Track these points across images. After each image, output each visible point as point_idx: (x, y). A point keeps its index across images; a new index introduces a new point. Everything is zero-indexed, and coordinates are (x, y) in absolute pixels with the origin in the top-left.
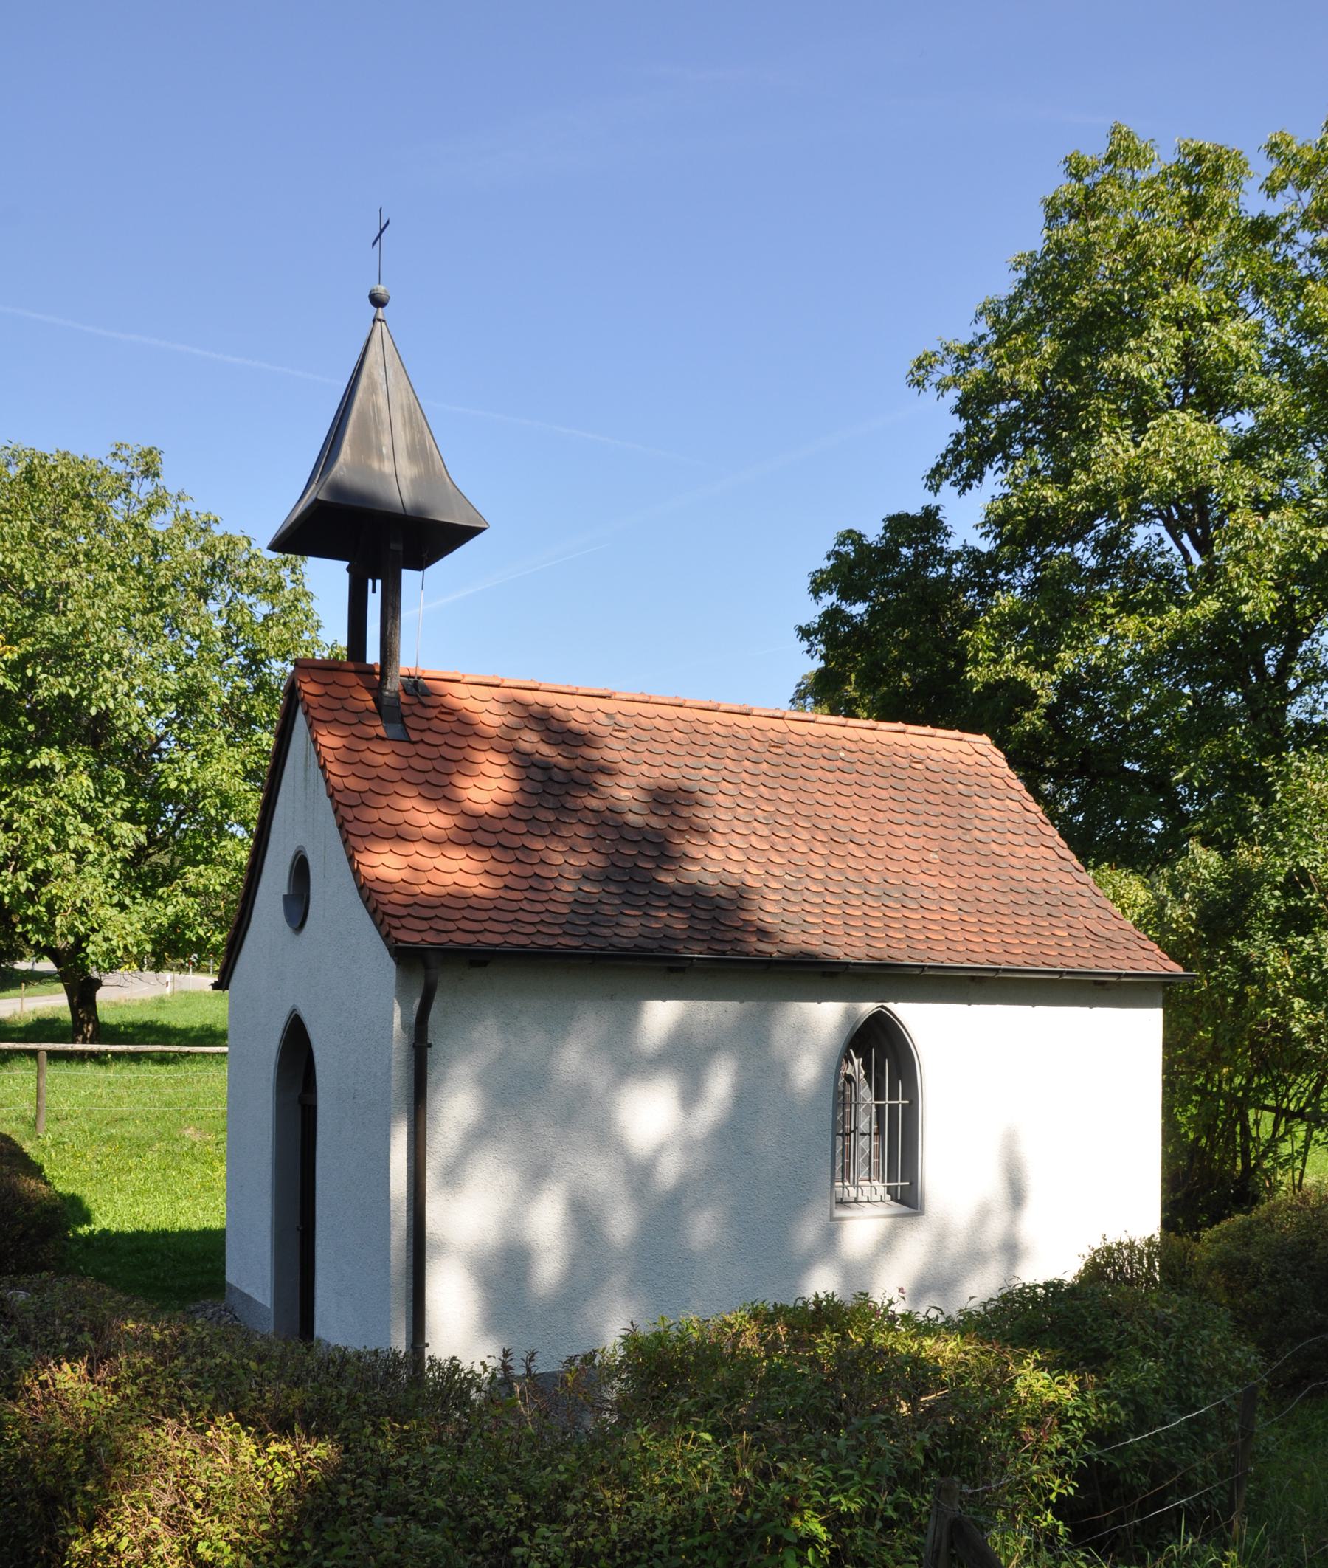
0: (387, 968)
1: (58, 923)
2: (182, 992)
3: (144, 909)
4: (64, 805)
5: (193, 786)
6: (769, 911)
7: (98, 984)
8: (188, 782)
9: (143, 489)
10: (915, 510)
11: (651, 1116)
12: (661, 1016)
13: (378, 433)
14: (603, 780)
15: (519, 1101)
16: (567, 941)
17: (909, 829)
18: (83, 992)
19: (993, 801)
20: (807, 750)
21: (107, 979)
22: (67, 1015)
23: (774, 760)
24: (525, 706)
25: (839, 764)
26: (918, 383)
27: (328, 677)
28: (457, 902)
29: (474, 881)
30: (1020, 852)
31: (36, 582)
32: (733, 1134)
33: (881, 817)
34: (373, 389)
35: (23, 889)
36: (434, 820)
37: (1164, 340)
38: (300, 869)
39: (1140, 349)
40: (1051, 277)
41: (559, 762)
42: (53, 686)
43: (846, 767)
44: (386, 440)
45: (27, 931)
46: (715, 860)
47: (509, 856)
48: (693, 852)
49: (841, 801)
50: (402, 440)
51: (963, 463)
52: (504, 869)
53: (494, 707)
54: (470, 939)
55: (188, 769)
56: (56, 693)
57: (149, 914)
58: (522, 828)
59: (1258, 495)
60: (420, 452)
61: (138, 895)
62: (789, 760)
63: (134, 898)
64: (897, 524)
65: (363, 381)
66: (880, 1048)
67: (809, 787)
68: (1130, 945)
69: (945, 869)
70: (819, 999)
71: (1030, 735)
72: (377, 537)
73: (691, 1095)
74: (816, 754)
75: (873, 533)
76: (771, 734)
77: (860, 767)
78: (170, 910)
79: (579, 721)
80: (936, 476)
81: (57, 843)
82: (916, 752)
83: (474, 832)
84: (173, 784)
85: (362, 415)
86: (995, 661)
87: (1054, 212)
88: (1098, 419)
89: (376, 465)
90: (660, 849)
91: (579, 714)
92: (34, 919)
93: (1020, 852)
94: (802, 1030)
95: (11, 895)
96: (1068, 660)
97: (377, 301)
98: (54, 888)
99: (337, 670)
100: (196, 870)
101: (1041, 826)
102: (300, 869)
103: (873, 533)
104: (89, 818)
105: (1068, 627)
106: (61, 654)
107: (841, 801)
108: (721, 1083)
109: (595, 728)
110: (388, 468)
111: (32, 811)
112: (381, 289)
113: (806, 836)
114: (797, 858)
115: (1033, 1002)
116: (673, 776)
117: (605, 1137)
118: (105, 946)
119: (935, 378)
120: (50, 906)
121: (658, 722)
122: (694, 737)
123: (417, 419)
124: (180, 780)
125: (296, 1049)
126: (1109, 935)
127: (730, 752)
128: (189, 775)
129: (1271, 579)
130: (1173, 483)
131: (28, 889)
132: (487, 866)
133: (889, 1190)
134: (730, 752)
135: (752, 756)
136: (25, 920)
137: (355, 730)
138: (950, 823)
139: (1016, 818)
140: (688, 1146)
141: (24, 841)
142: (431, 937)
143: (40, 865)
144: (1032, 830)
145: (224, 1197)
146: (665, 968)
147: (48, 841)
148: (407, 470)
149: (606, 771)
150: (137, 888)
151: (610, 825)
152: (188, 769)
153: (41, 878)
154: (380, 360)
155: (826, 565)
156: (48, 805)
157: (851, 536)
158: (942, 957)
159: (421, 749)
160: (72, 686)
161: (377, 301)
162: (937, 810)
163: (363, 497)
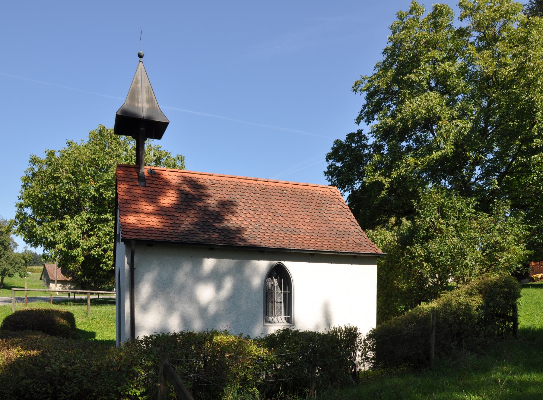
6: (246, 235)
10: (355, 131)
11: (206, 293)
12: (209, 263)
13: (138, 95)
14: (204, 198)
15: (163, 288)
16: (176, 239)
17: (302, 213)
19: (333, 205)
20: (274, 191)
23: (262, 193)
24: (185, 177)
25: (283, 194)
26: (355, 90)
27: (125, 169)
28: (150, 229)
29: (158, 224)
30: (338, 220)
32: (233, 299)
33: (293, 209)
36: (149, 208)
37: (426, 68)
39: (417, 72)
40: (392, 53)
41: (193, 193)
43: (285, 195)
44: (140, 97)
46: (233, 221)
47: (168, 218)
48: (227, 218)
49: (281, 205)
50: (145, 96)
51: (367, 115)
52: (165, 221)
53: (175, 178)
58: (174, 210)
59: (453, 116)
60: (150, 101)
62: (267, 193)
64: (351, 136)
66: (281, 275)
68: (367, 246)
69: (310, 224)
70: (259, 259)
71: (383, 197)
72: (139, 126)
73: (219, 288)
74: (276, 191)
75: (343, 139)
76: (263, 186)
77: (290, 195)
79: (201, 181)
80: (358, 120)
82: (310, 191)
83: (162, 212)
86: (373, 176)
87: (394, 29)
88: (405, 97)
89: (136, 105)
90: (218, 217)
91: (202, 180)
93: (338, 220)
94: (255, 270)
96: (394, 174)
97: (140, 56)
99: (129, 167)
101: (348, 213)
103: (343, 139)
105: (395, 163)
107: (281, 205)
108: (228, 284)
109: (205, 184)
110: (140, 105)
112: (141, 52)
113: (265, 214)
114: (261, 220)
115: (332, 262)
116: (227, 197)
117: (193, 299)
119: (360, 88)
121: (227, 183)
122: (237, 187)
123: (150, 90)
126: (360, 243)
127: (248, 191)
129: (452, 142)
130: (425, 114)
132: (160, 220)
133: (285, 318)
134: (248, 191)
135: (254, 192)
137: (130, 183)
138: (316, 211)
139: (340, 210)
140: (218, 302)
144: (344, 213)
145: (174, 326)
148: (146, 106)
149: (208, 196)
151: (205, 210)
154: (140, 74)
155: (331, 151)
157: (337, 142)
158: (299, 247)
159: (149, 189)
161: (140, 56)
162: (313, 207)
163: (134, 114)
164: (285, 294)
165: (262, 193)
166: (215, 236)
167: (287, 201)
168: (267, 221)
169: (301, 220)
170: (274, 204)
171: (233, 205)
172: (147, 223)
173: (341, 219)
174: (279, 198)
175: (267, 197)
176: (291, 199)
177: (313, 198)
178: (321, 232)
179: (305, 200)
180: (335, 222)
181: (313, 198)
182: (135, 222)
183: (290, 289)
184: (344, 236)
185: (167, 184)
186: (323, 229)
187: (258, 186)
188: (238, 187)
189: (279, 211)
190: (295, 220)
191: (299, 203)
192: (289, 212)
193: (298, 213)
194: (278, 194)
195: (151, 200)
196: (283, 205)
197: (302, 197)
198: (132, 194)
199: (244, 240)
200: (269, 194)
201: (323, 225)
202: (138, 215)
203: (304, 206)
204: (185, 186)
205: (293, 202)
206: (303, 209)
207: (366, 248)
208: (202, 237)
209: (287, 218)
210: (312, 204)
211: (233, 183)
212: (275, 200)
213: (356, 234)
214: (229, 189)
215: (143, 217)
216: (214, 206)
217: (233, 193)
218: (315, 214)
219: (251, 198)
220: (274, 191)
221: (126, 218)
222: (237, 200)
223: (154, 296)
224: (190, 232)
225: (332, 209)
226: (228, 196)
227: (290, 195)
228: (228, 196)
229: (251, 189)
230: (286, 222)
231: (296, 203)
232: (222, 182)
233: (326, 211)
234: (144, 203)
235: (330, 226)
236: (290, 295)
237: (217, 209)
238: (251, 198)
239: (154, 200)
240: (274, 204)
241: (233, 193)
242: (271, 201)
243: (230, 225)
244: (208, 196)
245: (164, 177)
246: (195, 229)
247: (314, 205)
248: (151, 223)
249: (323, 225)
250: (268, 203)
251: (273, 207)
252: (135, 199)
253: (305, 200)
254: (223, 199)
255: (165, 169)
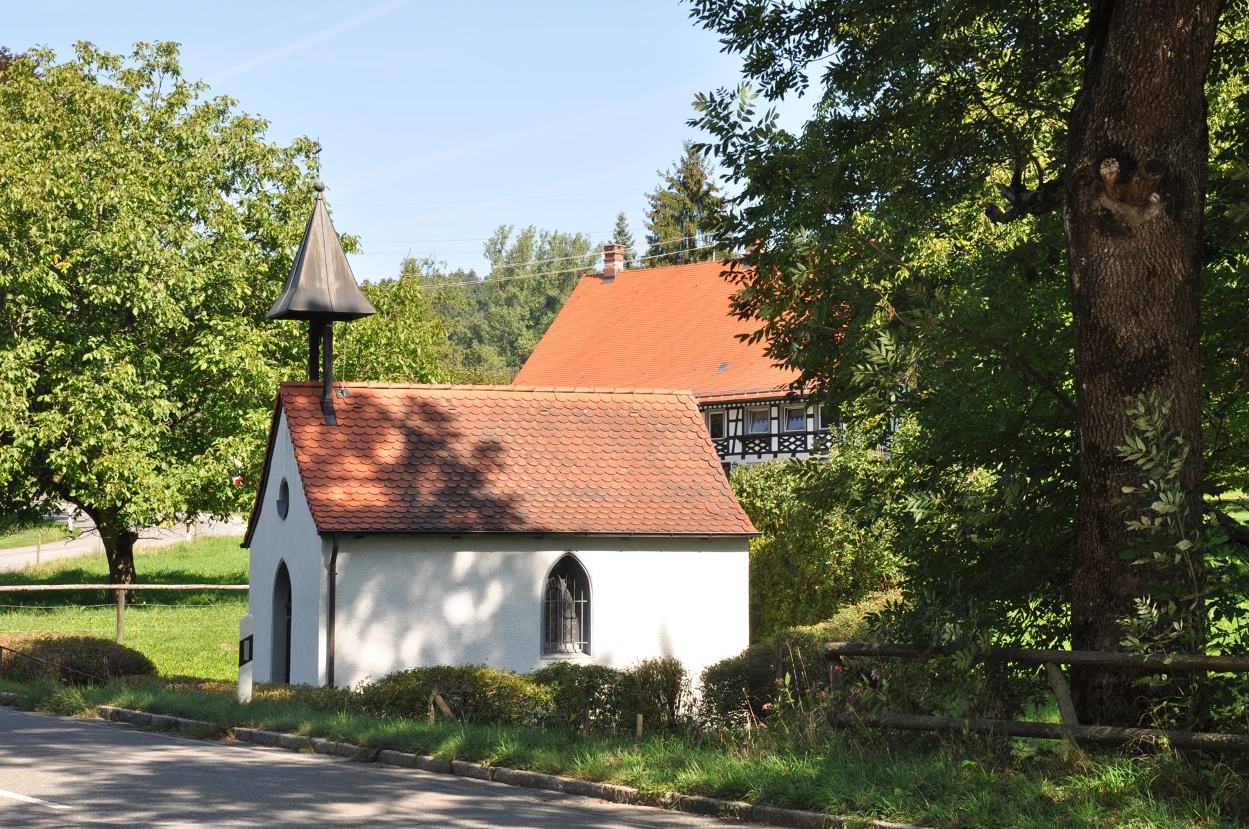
0: (318, 540)
1: (108, 490)
2: (205, 538)
3: (181, 473)
4: (114, 392)
5: (222, 366)
6: (523, 510)
7: (134, 537)
8: (217, 363)
9: (166, 85)
12: (464, 560)
13: (319, 266)
14: (449, 439)
17: (614, 455)
18: (120, 544)
20: (564, 411)
21: (143, 533)
22: (104, 569)
23: (543, 419)
24: (412, 399)
25: (582, 418)
28: (369, 510)
30: (683, 464)
31: (83, 203)
32: (502, 615)
33: (598, 449)
34: (316, 242)
35: (78, 461)
38: (285, 487)
42: (106, 294)
44: (323, 269)
45: (81, 496)
46: (499, 485)
50: (331, 270)
52: (391, 491)
54: (354, 526)
55: (217, 352)
56: (104, 300)
57: (184, 477)
61: (174, 461)
63: (170, 464)
65: (311, 237)
66: (570, 576)
67: (559, 434)
73: (480, 597)
76: (544, 403)
78: (202, 473)
81: (107, 424)
82: (636, 406)
84: (204, 366)
85: (311, 258)
90: (474, 477)
92: (85, 486)
93: (683, 464)
95: (68, 466)
98: (105, 461)
100: (226, 441)
102: (285, 487)
104: (134, 398)
106: (110, 265)
108: (495, 593)
110: (324, 286)
111: (85, 396)
114: (538, 477)
115: (661, 549)
118: (145, 506)
120: (100, 476)
121: (477, 402)
124: (210, 362)
125: (283, 575)
128: (218, 358)
131: (82, 462)
134: (515, 417)
135: (527, 417)
136: (81, 486)
138: (643, 449)
139: (690, 443)
141: (78, 421)
142: (337, 526)
143: (92, 442)
144: (699, 450)
146: (461, 537)
147: (100, 421)
149: (456, 436)
150: (173, 454)
152: (217, 352)
153: (94, 452)
156: (100, 391)
160: (118, 294)
164: (578, 605)
165: (543, 419)
166: (472, 515)
167: (588, 433)
168: (550, 477)
169: (612, 471)
170: (563, 440)
171: (500, 449)
172: (362, 497)
173: (690, 464)
174: (574, 427)
175: (550, 426)
176: (596, 427)
177: (639, 420)
178: (647, 493)
179: (624, 426)
180: (677, 471)
181: (639, 420)
182: (342, 496)
183: (587, 597)
184: (690, 499)
185: (384, 415)
186: (651, 486)
187: (535, 404)
188: (498, 410)
189: (571, 456)
190: (600, 471)
191: (611, 433)
192: (590, 455)
193: (607, 456)
194: (572, 418)
195: (362, 453)
196: (579, 441)
197: (618, 419)
198: (330, 444)
199: (520, 520)
200: (555, 419)
201: (653, 478)
202: (346, 483)
203: (620, 440)
204: (416, 417)
205: (600, 433)
206: (618, 448)
207: (728, 523)
208: (452, 518)
209: (585, 469)
210: (636, 435)
211: (489, 402)
212: (565, 433)
213: (714, 492)
214: (482, 417)
215: (354, 487)
216: (468, 454)
217: (490, 424)
218: (639, 456)
219: (521, 431)
220: (564, 411)
221: (329, 490)
222: (509, 439)
223: (375, 616)
224: (432, 509)
225: (676, 442)
226: (479, 432)
227: (595, 419)
228: (479, 432)
229: (522, 411)
230: (583, 477)
231: (605, 435)
232: (468, 403)
233: (662, 448)
234: (351, 459)
235: (666, 479)
236: (587, 606)
237: (475, 462)
238: (521, 431)
239: (366, 452)
240: (563, 440)
241: (490, 424)
242: (559, 434)
243: (496, 491)
244: (456, 436)
245: (377, 401)
246: (439, 503)
247: (640, 435)
248: (368, 497)
249: (653, 478)
250: (553, 441)
251: (562, 448)
252: (336, 454)
253: (624, 426)
254: (485, 438)
255: (386, 385)
